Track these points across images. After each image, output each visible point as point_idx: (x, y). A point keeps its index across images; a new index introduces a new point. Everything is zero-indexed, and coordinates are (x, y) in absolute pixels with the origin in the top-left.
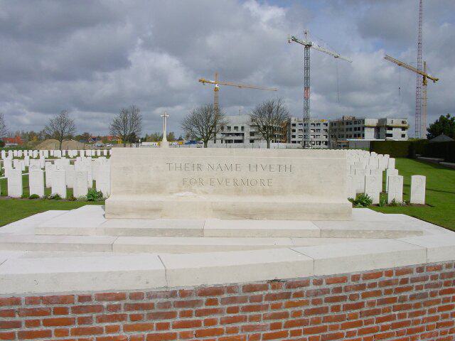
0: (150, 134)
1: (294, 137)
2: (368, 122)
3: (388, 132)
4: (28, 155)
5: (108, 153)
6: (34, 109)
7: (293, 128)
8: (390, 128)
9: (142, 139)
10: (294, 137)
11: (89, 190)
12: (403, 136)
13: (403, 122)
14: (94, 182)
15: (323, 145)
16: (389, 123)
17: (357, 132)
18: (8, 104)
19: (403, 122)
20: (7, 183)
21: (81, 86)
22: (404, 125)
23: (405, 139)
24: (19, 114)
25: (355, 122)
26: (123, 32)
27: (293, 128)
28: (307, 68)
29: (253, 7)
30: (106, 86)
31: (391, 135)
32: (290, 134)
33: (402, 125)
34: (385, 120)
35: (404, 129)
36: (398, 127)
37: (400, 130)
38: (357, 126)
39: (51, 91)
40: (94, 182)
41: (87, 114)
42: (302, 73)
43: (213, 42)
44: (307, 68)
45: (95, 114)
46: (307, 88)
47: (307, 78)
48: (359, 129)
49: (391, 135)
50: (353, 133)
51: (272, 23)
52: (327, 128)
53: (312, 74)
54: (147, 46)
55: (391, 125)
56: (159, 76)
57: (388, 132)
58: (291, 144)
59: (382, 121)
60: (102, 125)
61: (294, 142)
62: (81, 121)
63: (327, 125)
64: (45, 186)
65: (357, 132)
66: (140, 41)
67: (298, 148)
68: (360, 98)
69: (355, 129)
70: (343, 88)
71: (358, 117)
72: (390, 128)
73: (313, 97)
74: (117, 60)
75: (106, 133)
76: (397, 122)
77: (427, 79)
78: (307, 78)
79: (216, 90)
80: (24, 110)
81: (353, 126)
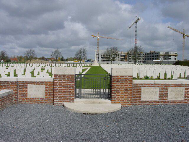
0: (69, 58)
1: (130, 59)
2: (161, 53)
3: (169, 57)
4: (5, 65)
5: (76, 65)
6: (21, 46)
7: (129, 55)
8: (170, 56)
9: (66, 59)
10: (130, 59)
11: (158, 76)
12: (175, 59)
13: (175, 54)
14: (159, 74)
15: (142, 63)
16: (169, 54)
17: (156, 57)
18: (10, 44)
19: (175, 54)
20: (32, 76)
21: (42, 36)
22: (176, 55)
23: (176, 60)
24: (14, 48)
25: (156, 53)
26: (62, 14)
27: (129, 55)
28: (136, 31)
29: (118, 3)
30: (52, 37)
31: (170, 59)
32: (128, 58)
33: (175, 55)
34: (168, 52)
35: (175, 56)
36: (173, 56)
37: (174, 56)
38: (156, 55)
39: (29, 39)
40: (159, 74)
41: (42, 48)
42: (134, 33)
43: (100, 18)
44: (136, 31)
45: (45, 49)
46: (136, 39)
47: (136, 35)
48: (157, 56)
49: (170, 59)
50: (155, 58)
51: (125, 10)
52: (144, 55)
53: (138, 32)
54: (73, 20)
55: (170, 55)
56: (75, 33)
57: (169, 57)
58: (130, 62)
59: (167, 53)
60: (48, 53)
61: (130, 61)
62: (39, 52)
63: (143, 54)
64: (171, 75)
65: (156, 57)
66: (70, 17)
67: (132, 64)
68: (158, 43)
69: (156, 56)
70: (154, 38)
71: (156, 51)
72: (170, 56)
73: (138, 42)
74: (59, 26)
75: (49, 57)
76: (173, 53)
77: (184, 36)
78: (136, 35)
79: (98, 39)
80: (17, 47)
81: (155, 55)
